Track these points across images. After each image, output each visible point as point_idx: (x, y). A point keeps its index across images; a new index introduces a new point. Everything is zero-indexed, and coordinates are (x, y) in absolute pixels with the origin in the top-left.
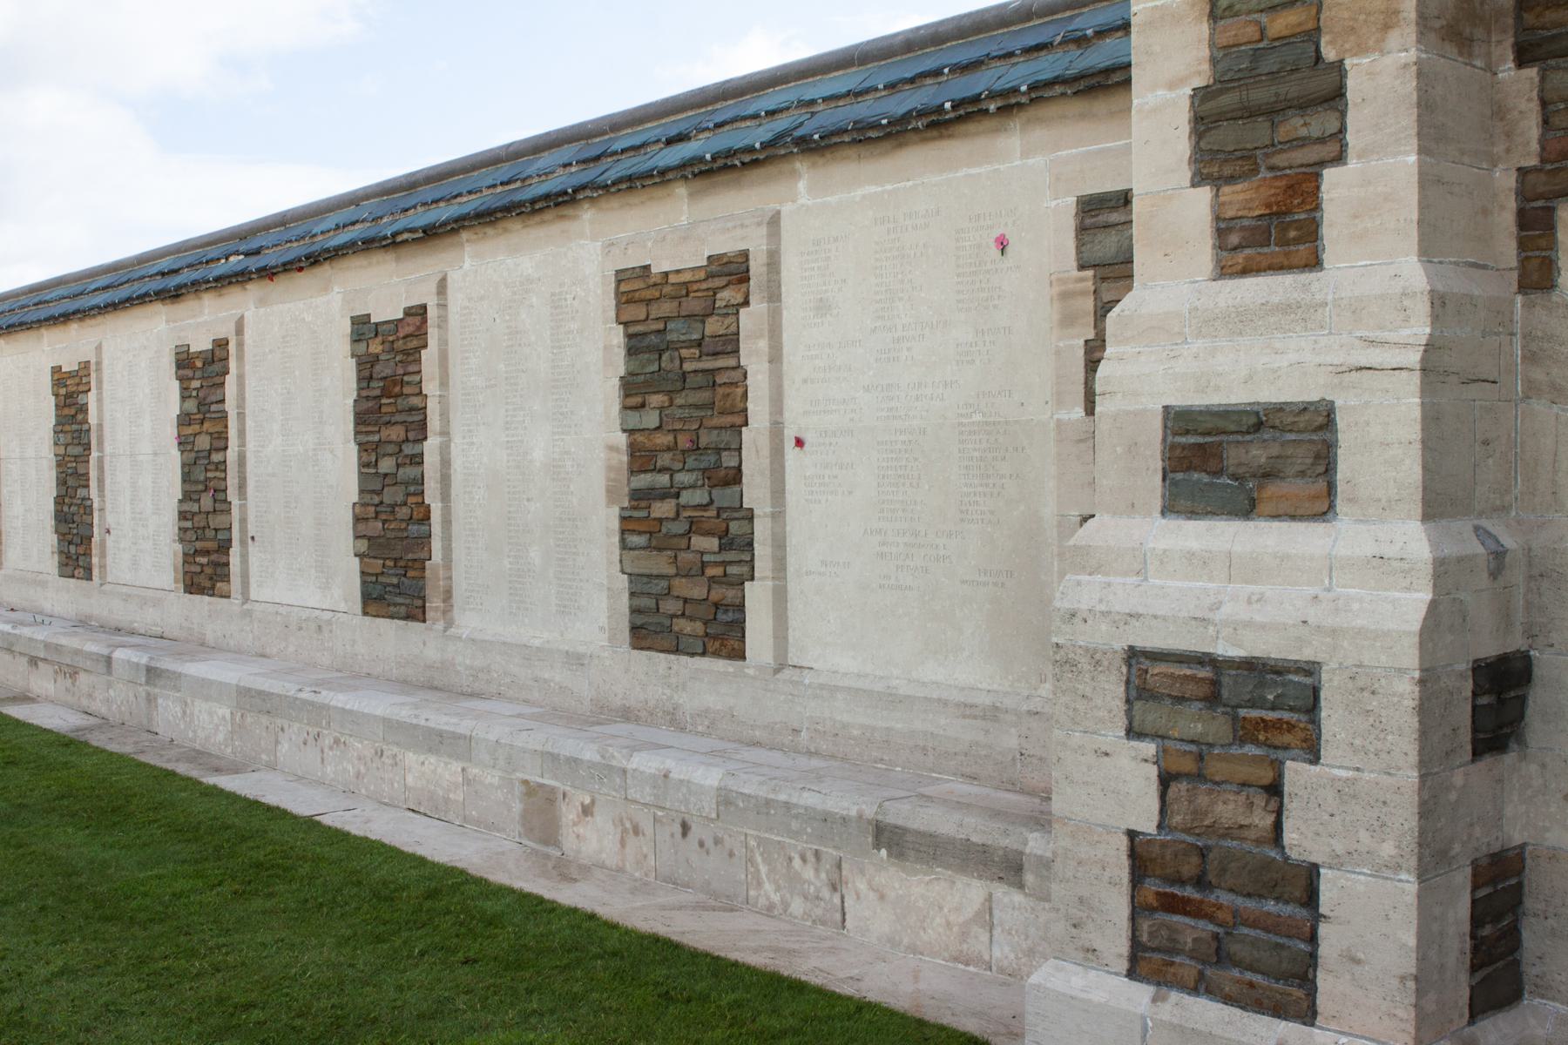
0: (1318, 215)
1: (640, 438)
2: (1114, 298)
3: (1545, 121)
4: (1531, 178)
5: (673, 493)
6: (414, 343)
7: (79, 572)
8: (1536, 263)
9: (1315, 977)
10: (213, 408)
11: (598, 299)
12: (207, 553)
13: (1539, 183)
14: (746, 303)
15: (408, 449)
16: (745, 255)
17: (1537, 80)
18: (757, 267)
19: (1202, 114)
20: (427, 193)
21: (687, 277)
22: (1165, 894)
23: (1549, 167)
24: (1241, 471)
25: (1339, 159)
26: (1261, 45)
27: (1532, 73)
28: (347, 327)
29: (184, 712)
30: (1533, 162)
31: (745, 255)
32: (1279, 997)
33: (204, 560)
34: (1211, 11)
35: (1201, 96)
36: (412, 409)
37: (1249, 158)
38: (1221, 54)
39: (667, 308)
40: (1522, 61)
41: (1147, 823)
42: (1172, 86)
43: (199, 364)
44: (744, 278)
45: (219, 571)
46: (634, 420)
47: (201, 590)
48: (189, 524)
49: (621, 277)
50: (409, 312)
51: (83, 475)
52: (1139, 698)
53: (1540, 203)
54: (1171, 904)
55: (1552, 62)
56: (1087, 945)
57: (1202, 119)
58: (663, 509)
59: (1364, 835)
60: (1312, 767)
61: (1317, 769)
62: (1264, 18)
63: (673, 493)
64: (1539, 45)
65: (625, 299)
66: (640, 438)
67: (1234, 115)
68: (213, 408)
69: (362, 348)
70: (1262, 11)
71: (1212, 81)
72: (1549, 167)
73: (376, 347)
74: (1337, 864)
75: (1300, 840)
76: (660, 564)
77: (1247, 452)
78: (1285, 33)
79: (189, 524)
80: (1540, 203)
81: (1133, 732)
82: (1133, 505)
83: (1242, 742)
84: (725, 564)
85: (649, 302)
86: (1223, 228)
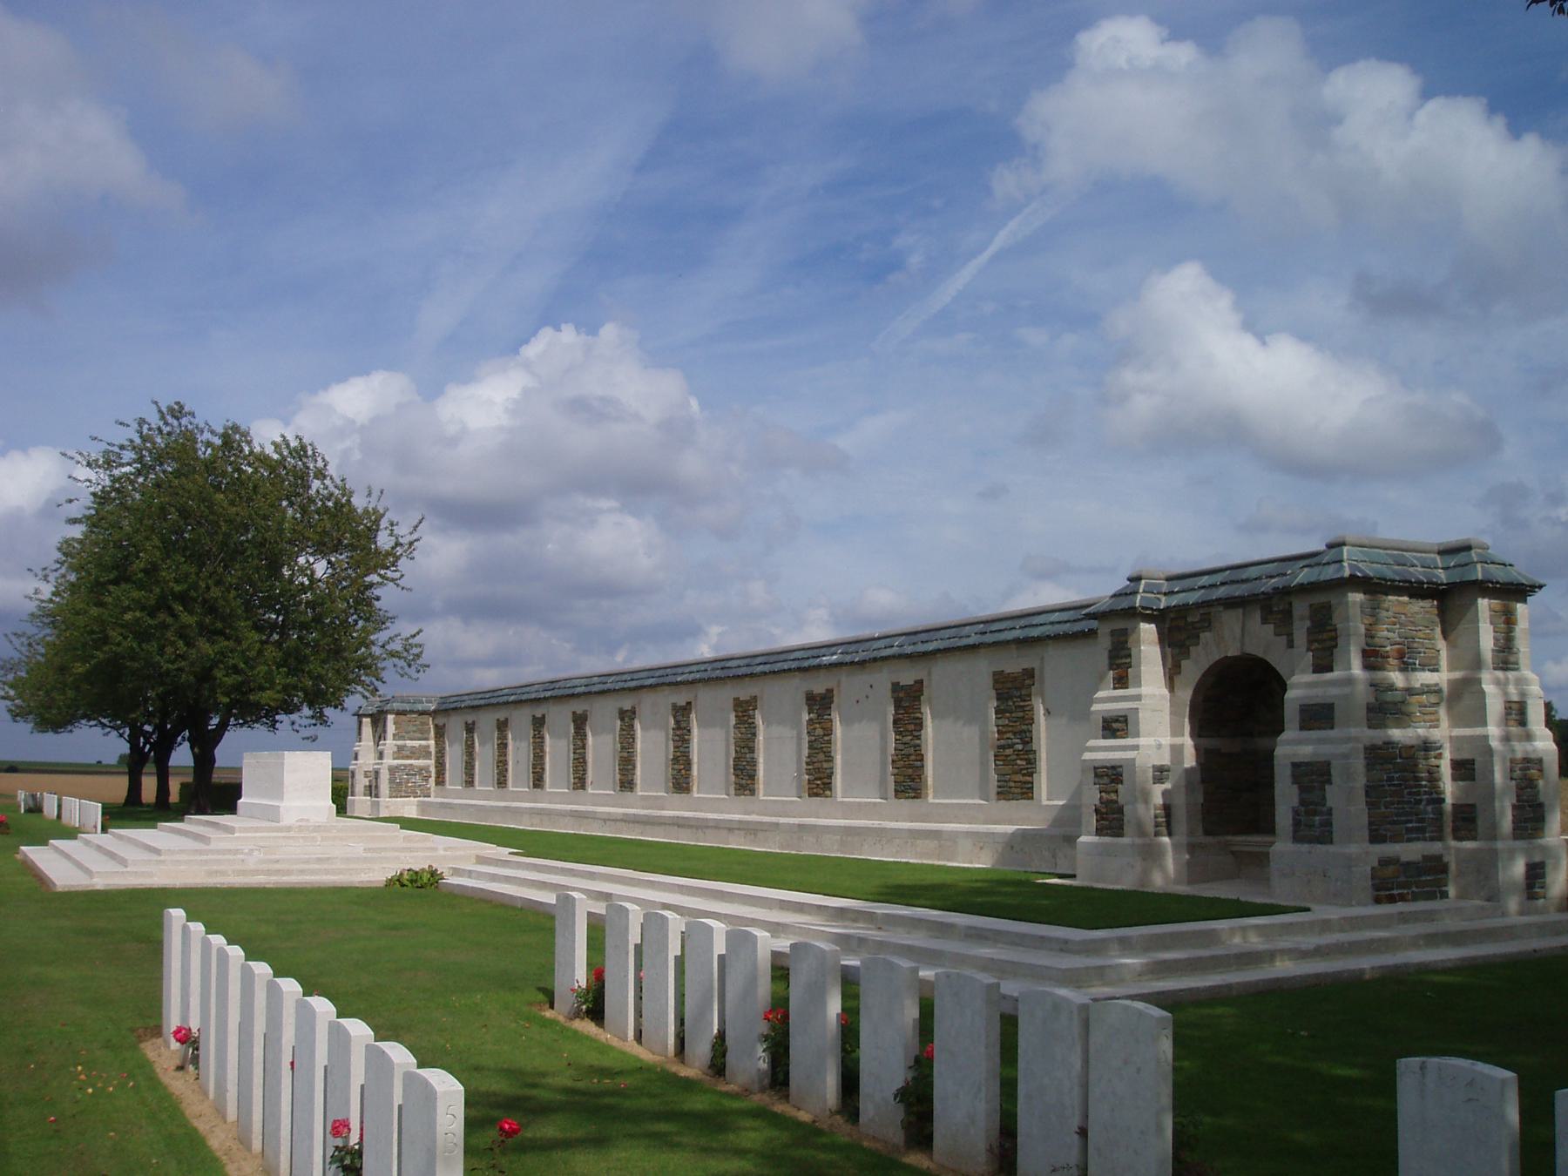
0: (1513, 634)
1: (1000, 728)
5: (1011, 746)
6: (919, 693)
7: (748, 792)
10: (826, 717)
11: (988, 682)
12: (820, 779)
14: (1033, 685)
15: (916, 734)
16: (1033, 669)
18: (1037, 673)
20: (924, 636)
21: (1016, 675)
25: (1131, 667)
28: (890, 686)
29: (817, 841)
31: (1033, 669)
33: (819, 782)
36: (918, 718)
38: (1113, 643)
39: (1010, 685)
43: (818, 699)
44: (1032, 676)
45: (826, 786)
46: (1000, 722)
47: (817, 795)
48: (810, 767)
49: (995, 673)
50: (916, 682)
54: (1103, 819)
58: (1009, 752)
63: (1011, 746)
65: (996, 681)
66: (1000, 728)
68: (826, 717)
69: (896, 695)
73: (901, 695)
75: (1121, 800)
76: (1008, 769)
79: (810, 767)
84: (1027, 768)
85: (1003, 682)
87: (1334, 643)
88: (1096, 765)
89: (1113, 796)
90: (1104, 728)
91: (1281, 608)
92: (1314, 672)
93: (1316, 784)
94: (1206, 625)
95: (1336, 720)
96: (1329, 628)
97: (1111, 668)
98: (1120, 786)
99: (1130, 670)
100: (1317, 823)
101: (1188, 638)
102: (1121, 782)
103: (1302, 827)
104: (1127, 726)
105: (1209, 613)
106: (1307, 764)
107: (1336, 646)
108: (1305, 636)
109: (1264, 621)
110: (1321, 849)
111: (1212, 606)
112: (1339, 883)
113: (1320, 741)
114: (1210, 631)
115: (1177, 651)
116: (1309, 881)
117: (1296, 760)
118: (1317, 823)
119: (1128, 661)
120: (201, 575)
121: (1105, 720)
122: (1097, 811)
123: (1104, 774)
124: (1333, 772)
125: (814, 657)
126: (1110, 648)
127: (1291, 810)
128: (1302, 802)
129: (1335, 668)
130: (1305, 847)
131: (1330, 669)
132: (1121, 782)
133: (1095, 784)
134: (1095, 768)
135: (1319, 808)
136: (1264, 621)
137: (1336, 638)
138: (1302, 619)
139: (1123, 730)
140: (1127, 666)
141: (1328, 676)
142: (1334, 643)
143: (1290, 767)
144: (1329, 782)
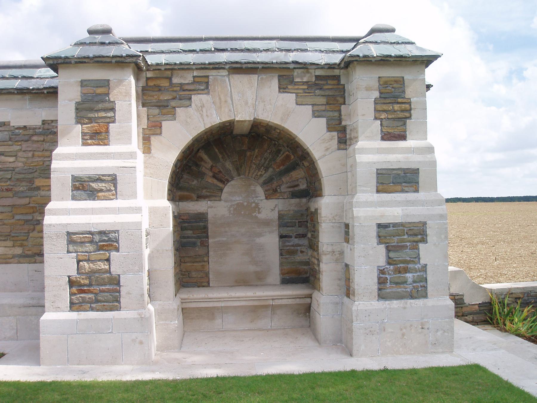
2: (395, 61)
3: (148, 119)
4: (146, 130)
8: (146, 148)
9: (120, 300)
13: (147, 132)
17: (147, 110)
19: (78, 108)
22: (79, 289)
23: (149, 128)
24: (92, 190)
25: (114, 122)
26: (94, 95)
27: (145, 109)
30: (146, 127)
32: (111, 306)
34: (81, 85)
35: (77, 103)
37: (91, 119)
38: (83, 94)
40: (143, 106)
41: (74, 273)
42: (70, 100)
51: (112, 102)
52: (70, 243)
53: (147, 136)
55: (150, 107)
56: (57, 306)
57: (78, 109)
59: (130, 266)
60: (118, 253)
61: (119, 253)
62: (95, 89)
64: (147, 103)
67: (87, 109)
70: (94, 87)
71: (81, 101)
72: (149, 128)
74: (125, 273)
75: (115, 270)
77: (400, 81)
78: (100, 93)
80: (147, 136)
81: (376, 118)
82: (63, 198)
83: (99, 250)
86: (84, 134)
87: (407, 115)
88: (71, 230)
89: (103, 266)
90: (75, 188)
91: (305, 80)
92: (383, 139)
93: (408, 244)
94: (202, 88)
95: (421, 184)
96: (400, 100)
97: (78, 122)
98: (114, 254)
99: (111, 125)
100: (410, 280)
101: (174, 99)
102: (117, 250)
103: (388, 285)
104: (115, 186)
105: (208, 77)
106: (395, 225)
107: (410, 117)
108: (372, 106)
109: (282, 89)
110: (420, 302)
111: (334, 68)
112: (439, 333)
113: (409, 203)
114: (208, 93)
115: (156, 111)
116: (403, 335)
117: (383, 221)
118: (410, 280)
119: (110, 114)
120: (287, 396)
121: (75, 179)
122: (72, 283)
123: (86, 240)
124: (429, 232)
125: (209, 51)
126: (79, 99)
127: (376, 270)
128: (390, 261)
129: (408, 136)
130: (395, 304)
131: (403, 137)
132: (117, 250)
133: (68, 252)
134: (68, 233)
135: (411, 266)
136: (282, 89)
137: (410, 110)
138: (368, 89)
139: (110, 190)
140: (108, 120)
141: (401, 144)
142: (407, 115)
143: (375, 228)
144: (424, 240)
